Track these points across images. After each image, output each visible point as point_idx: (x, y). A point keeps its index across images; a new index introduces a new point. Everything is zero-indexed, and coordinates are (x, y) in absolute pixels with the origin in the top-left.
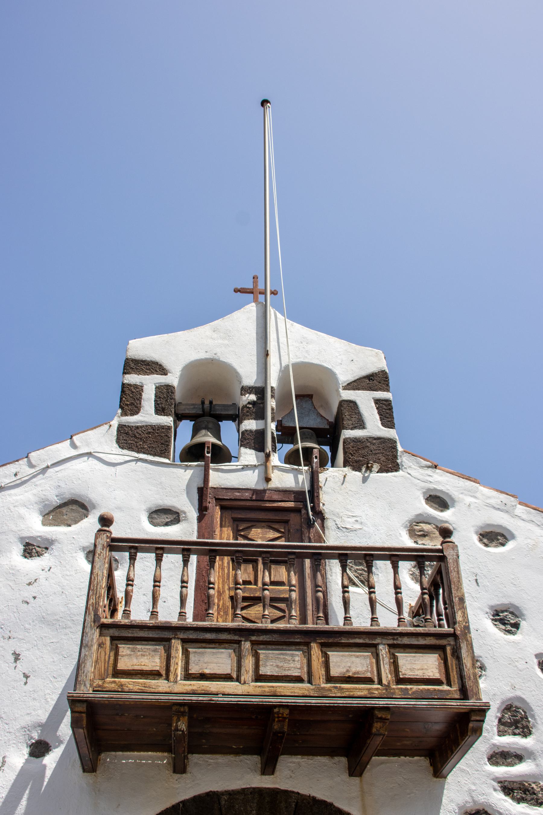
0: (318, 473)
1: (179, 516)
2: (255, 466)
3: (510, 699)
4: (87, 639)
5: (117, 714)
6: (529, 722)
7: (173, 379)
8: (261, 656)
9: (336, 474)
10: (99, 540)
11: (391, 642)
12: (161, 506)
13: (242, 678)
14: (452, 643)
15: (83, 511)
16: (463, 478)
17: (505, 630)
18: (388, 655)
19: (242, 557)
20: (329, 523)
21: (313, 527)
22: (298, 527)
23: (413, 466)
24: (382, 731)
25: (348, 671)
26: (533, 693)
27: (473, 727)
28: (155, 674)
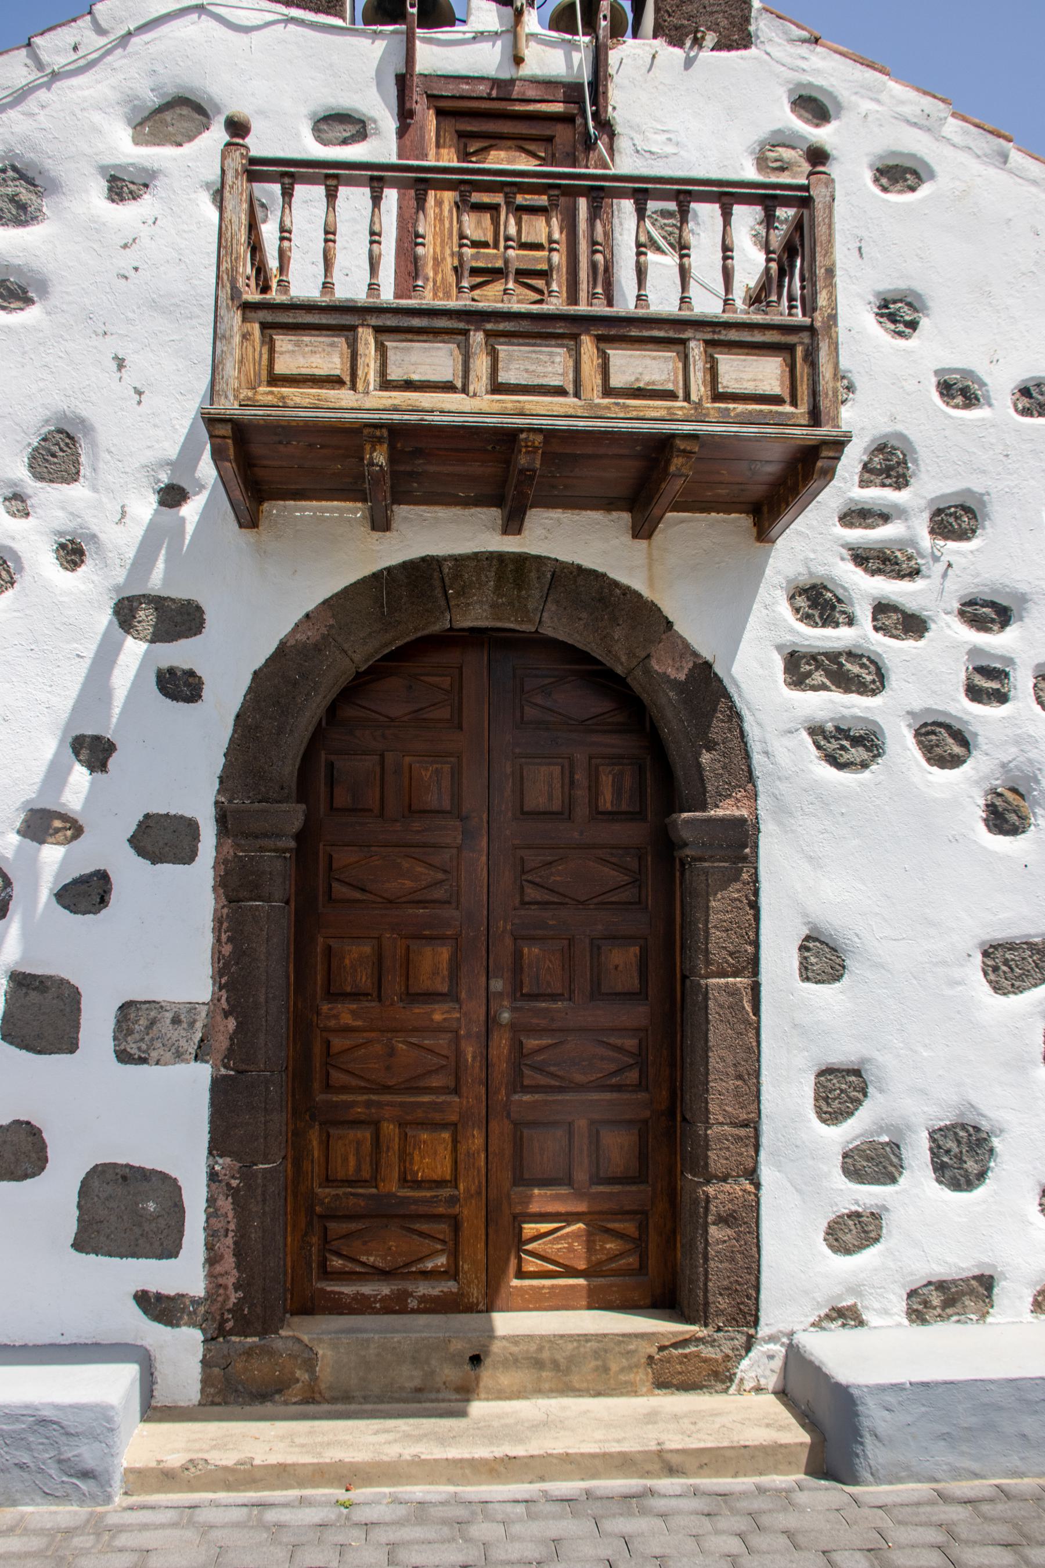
0: (607, 48)
1: (364, 127)
2: (496, 33)
3: (885, 436)
4: (223, 327)
5: (280, 443)
6: (908, 468)
8: (501, 355)
9: (639, 51)
10: (228, 161)
11: (709, 337)
12: (333, 109)
13: (471, 388)
14: (807, 341)
15: (201, 117)
16: (862, 64)
17: (894, 331)
18: (703, 357)
19: (467, 189)
20: (622, 143)
21: (594, 150)
22: (568, 149)
23: (776, 39)
24: (684, 471)
25: (637, 380)
26: (922, 427)
27: (822, 467)
28: (334, 381)
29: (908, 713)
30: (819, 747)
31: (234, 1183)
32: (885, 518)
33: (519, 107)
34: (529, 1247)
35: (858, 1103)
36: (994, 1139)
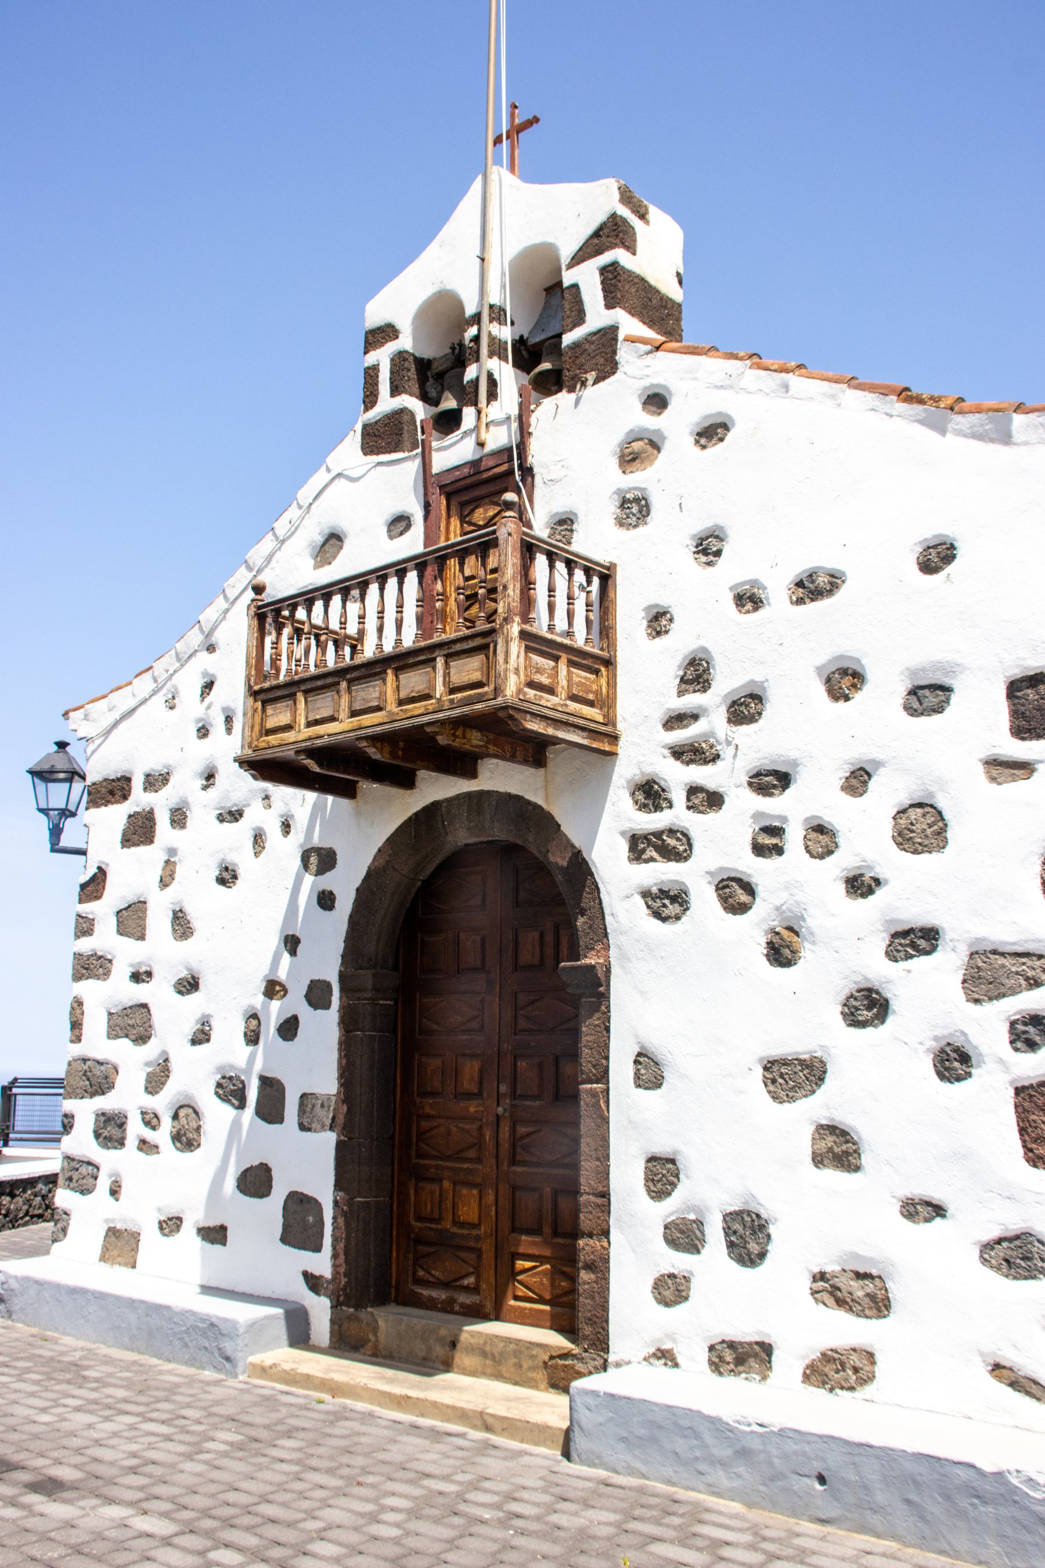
3: (693, 652)
7: (405, 342)
11: (445, 652)
28: (288, 728)
29: (707, 873)
30: (648, 907)
31: (345, 1208)
32: (695, 717)
33: (485, 476)
34: (519, 1278)
35: (674, 1185)
36: (771, 1226)
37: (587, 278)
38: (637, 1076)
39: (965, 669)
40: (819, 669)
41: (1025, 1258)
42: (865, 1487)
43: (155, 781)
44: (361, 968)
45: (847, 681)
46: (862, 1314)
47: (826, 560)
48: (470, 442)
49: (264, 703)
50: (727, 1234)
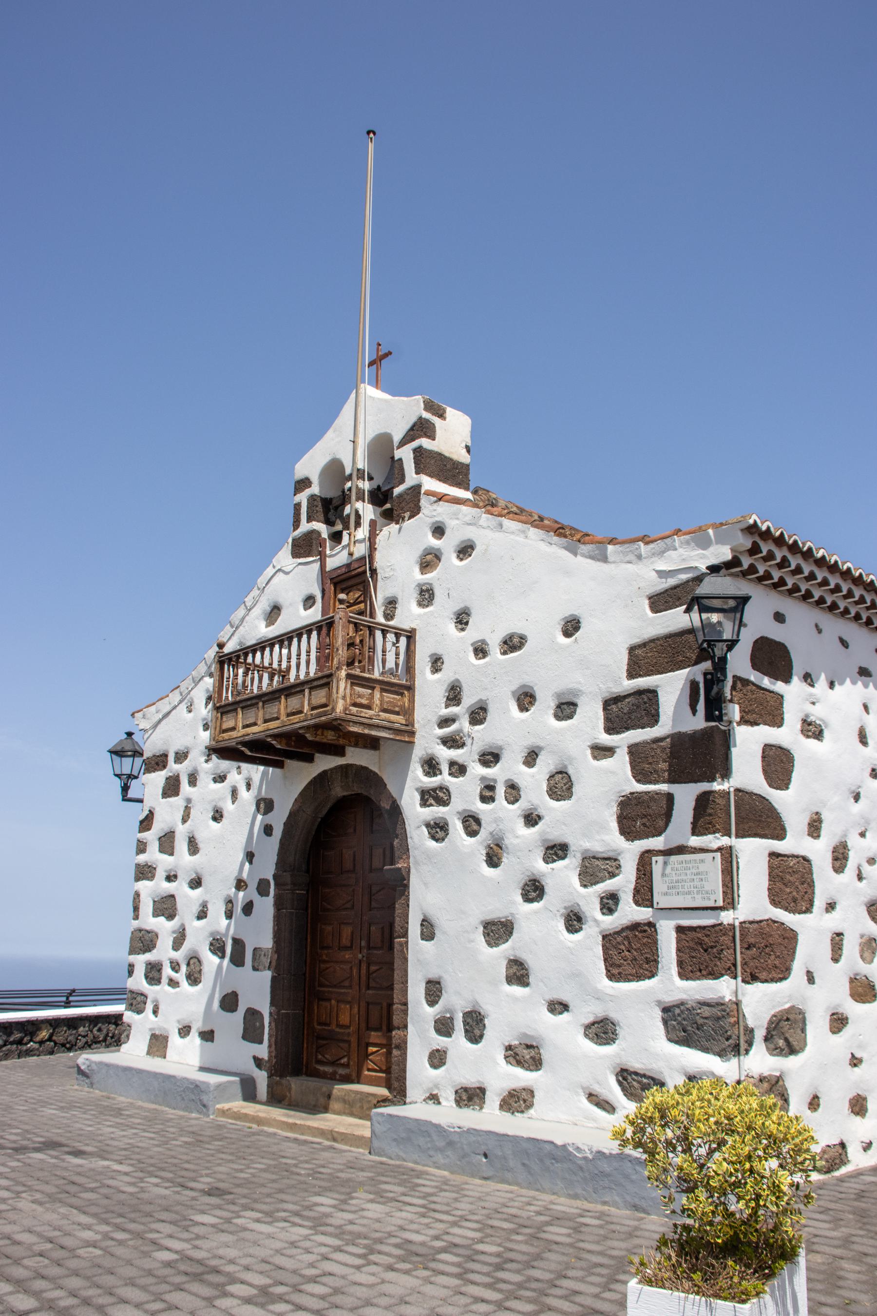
7: (315, 489)
28: (233, 729)
33: (353, 573)
35: (439, 997)
37: (406, 454)
38: (422, 933)
39: (583, 693)
40: (513, 693)
41: (605, 1033)
42: (505, 1158)
43: (181, 757)
44: (285, 871)
45: (528, 699)
46: (528, 1069)
47: (518, 628)
48: (345, 553)
49: (222, 714)
50: (464, 1025)
